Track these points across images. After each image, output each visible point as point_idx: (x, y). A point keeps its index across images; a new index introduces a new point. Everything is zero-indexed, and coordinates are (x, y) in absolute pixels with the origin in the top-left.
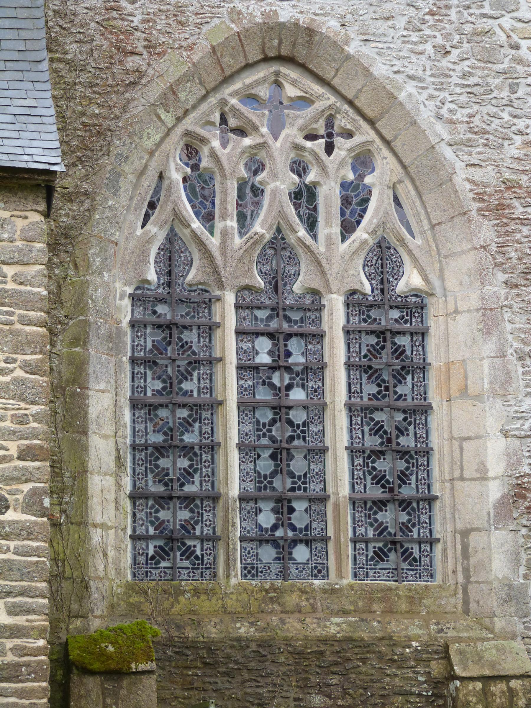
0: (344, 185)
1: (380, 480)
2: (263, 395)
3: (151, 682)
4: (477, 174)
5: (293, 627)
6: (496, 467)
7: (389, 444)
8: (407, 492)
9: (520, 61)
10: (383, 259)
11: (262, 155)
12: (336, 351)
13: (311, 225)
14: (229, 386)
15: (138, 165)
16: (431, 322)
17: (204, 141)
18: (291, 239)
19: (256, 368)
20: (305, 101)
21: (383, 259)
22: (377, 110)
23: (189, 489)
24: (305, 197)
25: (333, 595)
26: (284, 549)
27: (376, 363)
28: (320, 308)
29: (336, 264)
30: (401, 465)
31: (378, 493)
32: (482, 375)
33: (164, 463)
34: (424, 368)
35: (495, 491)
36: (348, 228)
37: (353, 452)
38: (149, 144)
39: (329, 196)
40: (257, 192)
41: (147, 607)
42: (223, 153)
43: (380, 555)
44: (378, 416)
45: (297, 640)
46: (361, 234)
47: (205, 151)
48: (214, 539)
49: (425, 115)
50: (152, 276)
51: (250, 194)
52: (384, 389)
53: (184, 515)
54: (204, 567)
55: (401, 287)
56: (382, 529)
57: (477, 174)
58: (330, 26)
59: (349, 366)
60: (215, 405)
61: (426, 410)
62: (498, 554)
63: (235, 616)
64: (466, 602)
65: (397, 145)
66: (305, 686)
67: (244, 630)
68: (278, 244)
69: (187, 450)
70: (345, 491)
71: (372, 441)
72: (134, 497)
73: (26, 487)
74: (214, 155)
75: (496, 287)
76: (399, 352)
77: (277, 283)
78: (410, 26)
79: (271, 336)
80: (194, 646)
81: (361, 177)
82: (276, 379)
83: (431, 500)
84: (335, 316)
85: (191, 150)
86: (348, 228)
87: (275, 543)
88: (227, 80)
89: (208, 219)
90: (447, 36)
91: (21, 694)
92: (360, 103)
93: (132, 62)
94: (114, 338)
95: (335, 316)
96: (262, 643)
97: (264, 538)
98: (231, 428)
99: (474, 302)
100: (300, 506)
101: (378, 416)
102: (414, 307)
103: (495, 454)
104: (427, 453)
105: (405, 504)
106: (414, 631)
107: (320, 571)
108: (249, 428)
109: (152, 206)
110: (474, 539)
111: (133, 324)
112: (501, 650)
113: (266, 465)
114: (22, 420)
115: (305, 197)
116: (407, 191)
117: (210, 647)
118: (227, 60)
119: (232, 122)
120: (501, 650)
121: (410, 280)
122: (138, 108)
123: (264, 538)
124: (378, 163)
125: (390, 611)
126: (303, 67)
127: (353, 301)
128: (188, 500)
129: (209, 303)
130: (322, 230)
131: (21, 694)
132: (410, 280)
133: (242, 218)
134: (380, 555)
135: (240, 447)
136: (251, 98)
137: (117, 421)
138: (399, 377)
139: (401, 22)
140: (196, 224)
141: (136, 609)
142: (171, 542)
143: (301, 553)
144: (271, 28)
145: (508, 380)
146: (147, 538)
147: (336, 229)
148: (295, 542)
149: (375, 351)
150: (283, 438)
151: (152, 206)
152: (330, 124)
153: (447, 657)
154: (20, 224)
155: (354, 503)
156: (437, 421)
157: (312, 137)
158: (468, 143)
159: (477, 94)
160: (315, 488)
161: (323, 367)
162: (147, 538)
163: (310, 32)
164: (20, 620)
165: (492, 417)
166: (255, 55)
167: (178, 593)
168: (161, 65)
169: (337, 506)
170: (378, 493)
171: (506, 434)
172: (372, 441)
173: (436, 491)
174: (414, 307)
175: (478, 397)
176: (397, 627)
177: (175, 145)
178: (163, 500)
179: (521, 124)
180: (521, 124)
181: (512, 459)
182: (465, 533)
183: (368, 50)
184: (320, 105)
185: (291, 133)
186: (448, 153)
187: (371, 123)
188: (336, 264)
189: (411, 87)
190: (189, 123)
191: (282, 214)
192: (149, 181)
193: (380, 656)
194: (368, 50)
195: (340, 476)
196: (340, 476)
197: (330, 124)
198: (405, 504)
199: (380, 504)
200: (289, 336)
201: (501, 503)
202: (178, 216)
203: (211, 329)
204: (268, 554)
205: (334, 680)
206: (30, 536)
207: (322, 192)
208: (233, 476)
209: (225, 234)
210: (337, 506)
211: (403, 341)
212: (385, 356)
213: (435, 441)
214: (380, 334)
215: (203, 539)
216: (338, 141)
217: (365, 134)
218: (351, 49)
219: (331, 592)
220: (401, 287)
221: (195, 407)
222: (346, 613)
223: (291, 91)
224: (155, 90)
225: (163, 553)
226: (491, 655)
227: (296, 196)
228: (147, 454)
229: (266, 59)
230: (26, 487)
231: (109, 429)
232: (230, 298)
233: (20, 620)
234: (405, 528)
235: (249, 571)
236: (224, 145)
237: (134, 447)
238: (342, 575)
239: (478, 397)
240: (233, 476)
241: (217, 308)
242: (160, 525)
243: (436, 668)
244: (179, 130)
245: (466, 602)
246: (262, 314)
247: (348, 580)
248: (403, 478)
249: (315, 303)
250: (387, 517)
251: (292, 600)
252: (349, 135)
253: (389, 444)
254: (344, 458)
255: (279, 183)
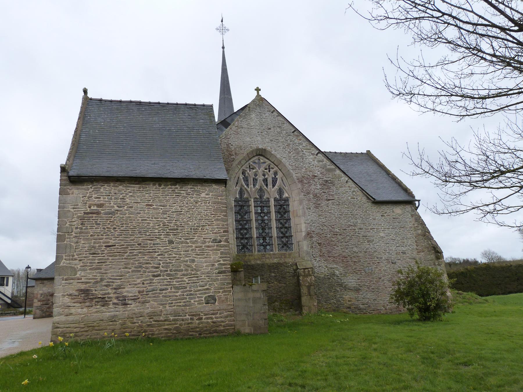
0: (272, 178)
1: (282, 233)
2: (259, 218)
3: (242, 273)
4: (297, 175)
5: (268, 261)
6: (304, 229)
7: (283, 226)
8: (287, 235)
9: (304, 154)
10: (280, 192)
11: (257, 173)
12: (273, 209)
13: (267, 185)
14: (253, 216)
15: (234, 176)
16: (290, 203)
17: (246, 171)
18: (263, 188)
19: (258, 213)
20: (264, 163)
21: (280, 192)
22: (278, 164)
23: (247, 236)
24: (265, 181)
25: (274, 255)
26: (265, 247)
27: (280, 211)
28: (269, 201)
29: (272, 193)
30: (286, 230)
31: (282, 235)
32: (300, 212)
33: (242, 231)
34: (289, 211)
35: (304, 234)
36: (274, 186)
37: (277, 228)
38: (236, 172)
39: (270, 180)
40: (256, 180)
41: (240, 259)
42: (250, 173)
43: (283, 247)
44: (281, 221)
45: (21, 297)
46: (276, 187)
47: (246, 173)
48: (252, 245)
49: (287, 164)
50: (238, 197)
51: (255, 180)
52: (282, 216)
53: (246, 241)
54: (250, 251)
55: (284, 196)
56: (283, 242)
57: (297, 175)
58: (269, 149)
59: (275, 212)
60: (251, 220)
61: (290, 219)
62: (305, 245)
63: (257, 260)
64: (299, 255)
65: (282, 170)
66: (271, 272)
67: (259, 262)
68: (261, 190)
69: (246, 229)
70: (276, 235)
71: (280, 226)
72: (236, 238)
73: (225, 238)
74: (248, 173)
75: (302, 196)
76: (284, 209)
77: (261, 197)
78: (283, 148)
79: (260, 207)
80: (249, 265)
81: (275, 176)
82: (262, 215)
83: (292, 236)
84: (272, 203)
85: (243, 173)
86: (274, 186)
87: (263, 246)
88: (250, 159)
89: (248, 185)
90: (290, 150)
91: (226, 276)
92: (275, 162)
93: (232, 157)
94: (231, 208)
95: (272, 203)
96: (263, 264)
97: (261, 245)
98: (254, 224)
99: (298, 199)
100: (267, 238)
101: (281, 221)
102: (287, 200)
103: (303, 227)
104: (290, 227)
105: (287, 237)
106: (290, 261)
107: (272, 250)
108: (257, 224)
109: (237, 183)
110: (300, 243)
111: (235, 206)
112: (306, 263)
113: (261, 231)
114: (223, 225)
115: (265, 181)
116: (284, 178)
117: (252, 265)
118: (250, 156)
119: (251, 167)
120: (306, 263)
121: (286, 195)
122: (234, 165)
123: (261, 245)
124: (278, 173)
125: (285, 257)
126: (264, 156)
127: (275, 200)
128: (246, 238)
129: (248, 201)
130: (269, 187)
131: (226, 276)
132: (286, 195)
133: (254, 185)
134: (283, 247)
135: (256, 228)
136: (254, 162)
137: (233, 224)
138: (285, 213)
139: (282, 148)
140: (245, 186)
141: (238, 259)
142: (244, 246)
143: (268, 247)
144: (258, 149)
145: (305, 213)
146: (239, 246)
147: (272, 186)
148: (267, 245)
149: (280, 209)
150: (264, 226)
151: (237, 183)
152: (269, 166)
153: (296, 265)
154: (221, 189)
155: (277, 237)
156: (292, 222)
157: (266, 169)
158: (295, 169)
159: (296, 160)
160: (270, 235)
161: (270, 212)
162: (239, 246)
163: (265, 150)
164: (225, 262)
165: (303, 220)
166: (255, 154)
167: (246, 256)
168: (238, 157)
169: (274, 238)
170: (282, 235)
171: (305, 223)
172: (280, 226)
173: (292, 234)
174: (287, 200)
175: (300, 217)
176: (287, 260)
177: (241, 172)
178: (242, 239)
179: (305, 165)
180: (305, 165)
181: (307, 228)
182: (298, 242)
183: (275, 153)
184: (267, 163)
185: (262, 169)
186: (292, 171)
187: (277, 166)
188: (272, 193)
189: (284, 159)
190: (244, 168)
191: (261, 184)
192: (236, 179)
193: (284, 266)
194: (275, 153)
195: (274, 232)
196: (274, 232)
197: (269, 166)
198: (287, 237)
199: (282, 237)
200: (264, 207)
201: (305, 236)
202: (242, 185)
203: (249, 206)
204: (262, 247)
205: (276, 270)
206: (226, 247)
207: (268, 180)
208: (255, 233)
209: (251, 188)
210: (274, 238)
211: (285, 207)
212: (282, 210)
213: (292, 225)
214: (281, 205)
215: (250, 246)
216: (271, 170)
217: (276, 168)
218: (273, 153)
219: (274, 254)
220: (284, 196)
221: (247, 221)
222: (277, 258)
223: (262, 161)
224: (236, 162)
225: (242, 248)
226: (305, 264)
227: (264, 180)
228: (238, 230)
229: (257, 155)
230: (225, 238)
231: (231, 226)
232: (252, 200)
233: (225, 262)
234: (287, 242)
235: (259, 251)
236: (250, 171)
237: (236, 229)
238: (276, 251)
239: (300, 217)
240: (255, 233)
241: (250, 202)
242: (242, 243)
243: (295, 267)
244: (242, 169)
245: (299, 255)
246: (259, 203)
247: (277, 252)
248: (286, 232)
249: (268, 200)
250: (284, 240)
251: (267, 256)
252: (273, 168)
253: (283, 226)
254: (275, 229)
255: (260, 178)
